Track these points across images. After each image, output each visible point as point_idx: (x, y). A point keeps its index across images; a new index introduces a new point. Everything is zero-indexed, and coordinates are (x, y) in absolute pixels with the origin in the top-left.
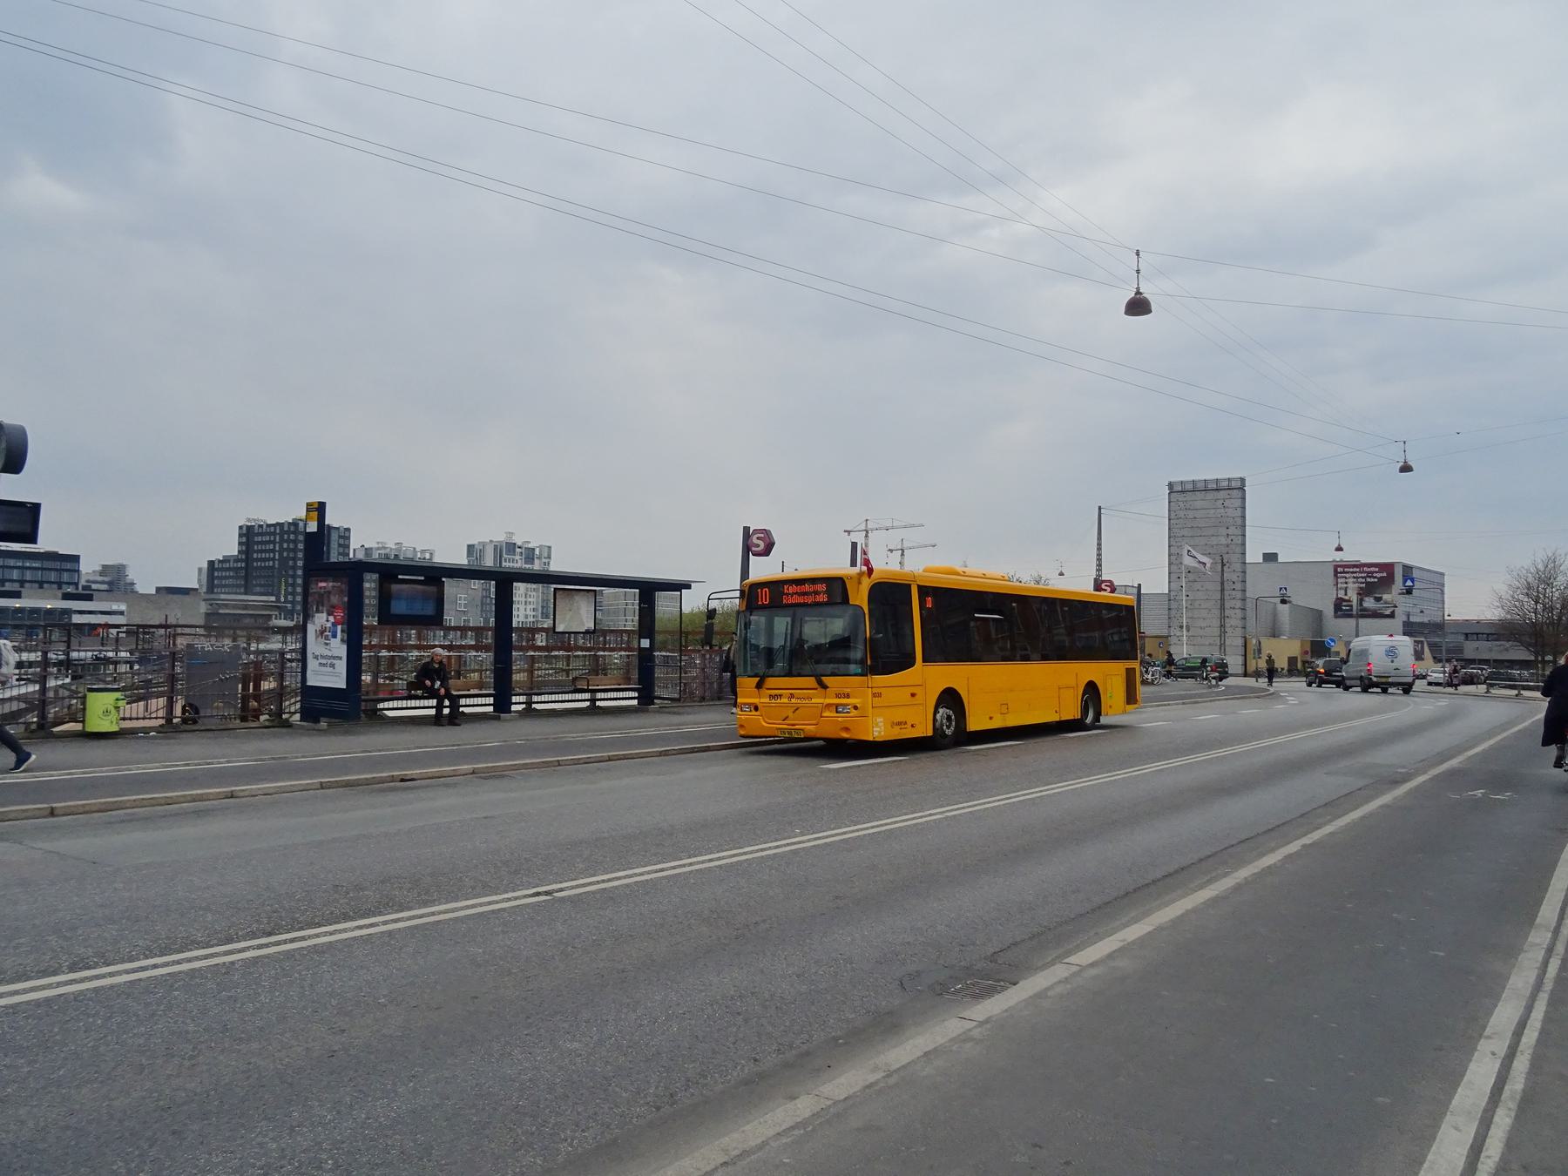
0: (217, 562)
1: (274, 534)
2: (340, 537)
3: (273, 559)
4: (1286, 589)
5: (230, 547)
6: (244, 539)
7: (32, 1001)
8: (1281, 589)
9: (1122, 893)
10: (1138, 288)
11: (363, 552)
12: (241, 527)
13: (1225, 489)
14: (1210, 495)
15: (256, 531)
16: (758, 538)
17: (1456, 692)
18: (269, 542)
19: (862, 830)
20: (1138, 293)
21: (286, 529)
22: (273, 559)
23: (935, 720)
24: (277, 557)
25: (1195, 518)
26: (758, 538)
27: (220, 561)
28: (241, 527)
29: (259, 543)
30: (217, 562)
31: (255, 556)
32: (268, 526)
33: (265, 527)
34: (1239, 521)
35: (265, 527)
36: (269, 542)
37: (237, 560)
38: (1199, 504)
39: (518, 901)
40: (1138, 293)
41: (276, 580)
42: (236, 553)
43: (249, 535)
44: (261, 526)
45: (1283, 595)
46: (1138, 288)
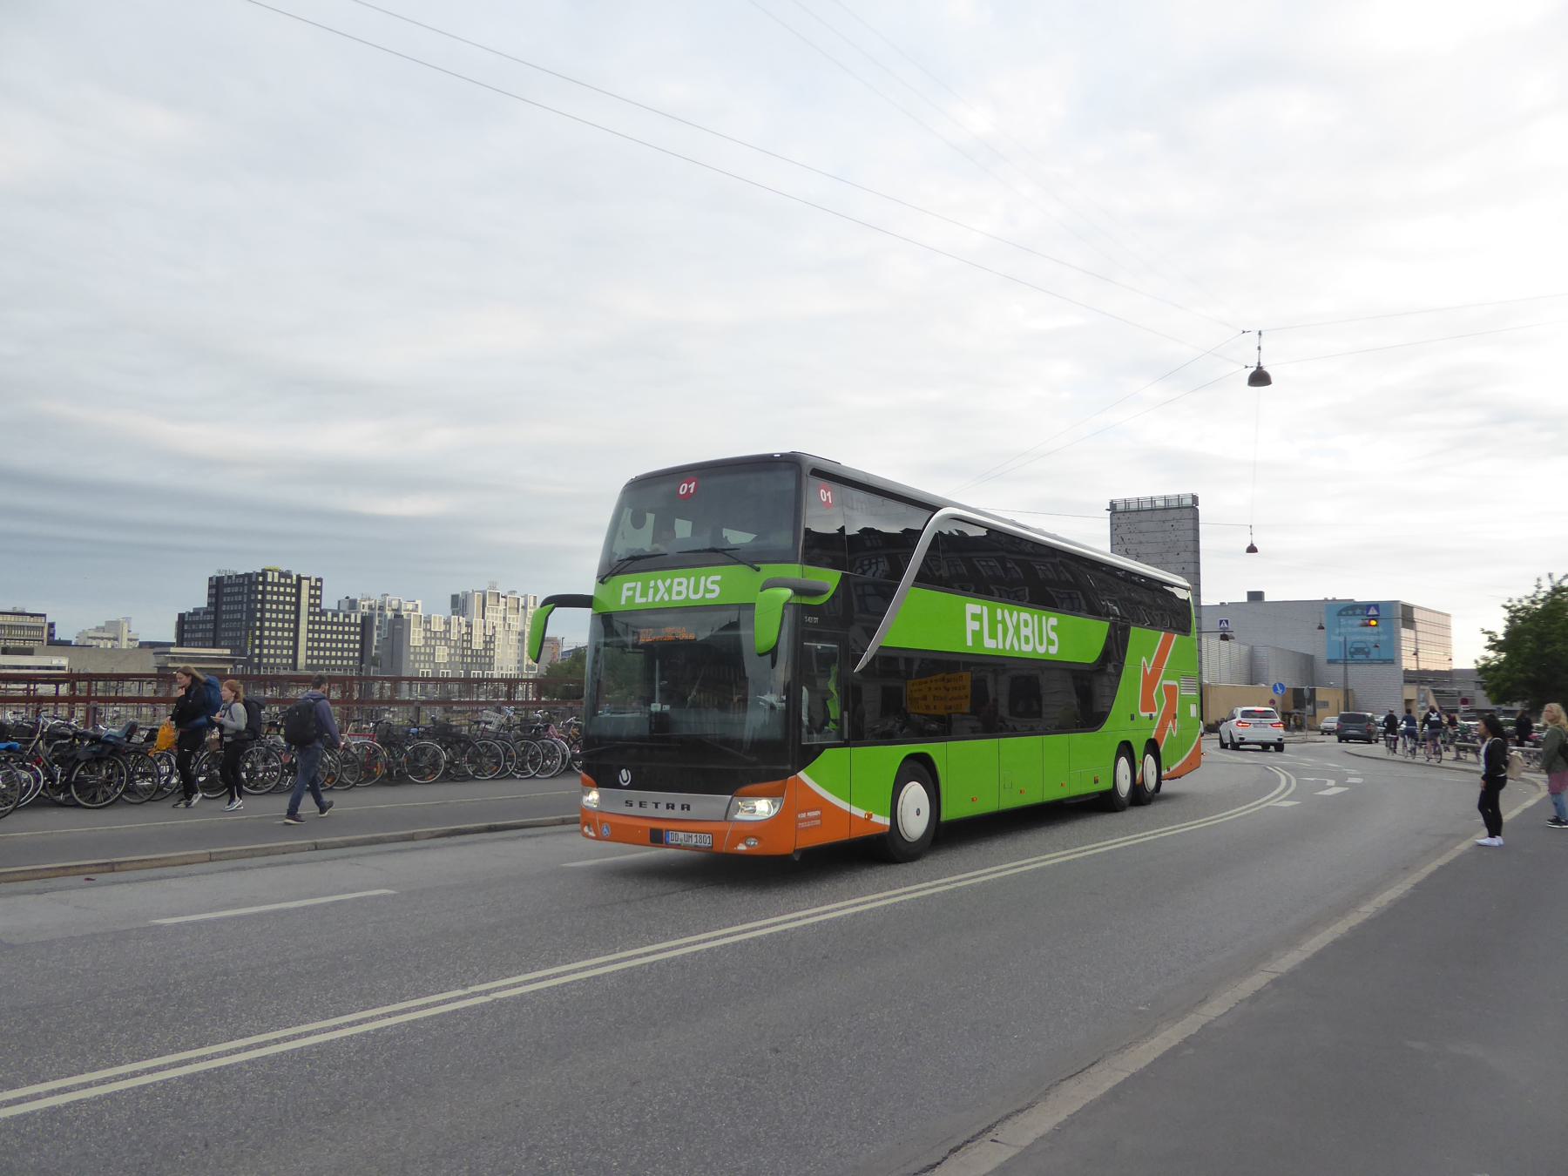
0: (187, 615)
1: (242, 585)
2: (311, 588)
3: (241, 611)
4: (1227, 621)
5: (199, 599)
6: (214, 591)
7: (38, 1110)
8: (1221, 622)
9: (1013, 1118)
10: (1259, 363)
11: (347, 604)
12: (211, 579)
13: (1174, 508)
14: (1159, 515)
15: (225, 582)
16: (714, 591)
17: (1413, 761)
18: (238, 593)
19: (1053, 858)
20: (1252, 545)
21: (254, 579)
22: (241, 611)
23: (592, 838)
24: (245, 609)
25: (1141, 543)
26: (714, 591)
27: (190, 614)
28: (211, 579)
29: (228, 595)
30: (187, 615)
31: (224, 608)
32: (237, 576)
33: (234, 578)
34: (1191, 545)
35: (234, 578)
36: (238, 593)
37: (206, 612)
38: (1144, 526)
39: (706, 944)
40: (1252, 545)
41: (243, 633)
42: (206, 606)
43: (218, 586)
44: (230, 577)
45: (1224, 630)
46: (1259, 363)
